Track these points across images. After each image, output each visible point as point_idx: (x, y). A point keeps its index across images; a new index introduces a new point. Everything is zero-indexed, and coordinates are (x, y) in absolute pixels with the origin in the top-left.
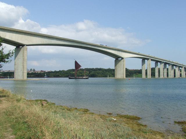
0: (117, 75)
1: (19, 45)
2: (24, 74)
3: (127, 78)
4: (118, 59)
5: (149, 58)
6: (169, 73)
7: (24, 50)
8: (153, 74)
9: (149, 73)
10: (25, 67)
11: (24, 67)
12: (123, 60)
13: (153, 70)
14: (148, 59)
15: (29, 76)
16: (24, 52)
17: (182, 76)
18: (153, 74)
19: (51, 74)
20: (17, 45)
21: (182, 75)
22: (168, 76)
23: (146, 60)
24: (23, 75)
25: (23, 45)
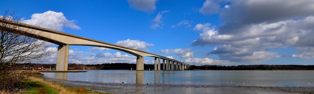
4: (138, 57)
7: (66, 48)
16: (66, 50)
25: (65, 45)
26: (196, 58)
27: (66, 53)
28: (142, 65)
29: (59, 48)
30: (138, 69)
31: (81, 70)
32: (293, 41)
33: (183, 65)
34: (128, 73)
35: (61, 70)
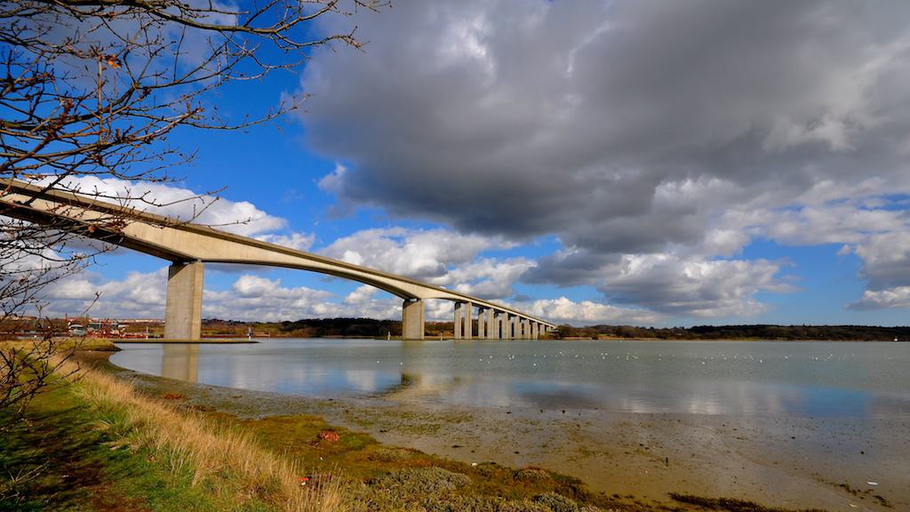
2: (194, 328)
3: (197, 322)
5: (469, 300)
6: (503, 330)
7: (195, 272)
8: (475, 333)
9: (469, 329)
10: (195, 311)
12: (419, 302)
13: (475, 324)
14: (466, 302)
15: (135, 334)
16: (194, 277)
18: (475, 333)
21: (525, 332)
22: (486, 335)
24: (190, 329)
25: (192, 260)
29: (172, 273)
30: (407, 337)
33: (535, 325)
35: (178, 337)
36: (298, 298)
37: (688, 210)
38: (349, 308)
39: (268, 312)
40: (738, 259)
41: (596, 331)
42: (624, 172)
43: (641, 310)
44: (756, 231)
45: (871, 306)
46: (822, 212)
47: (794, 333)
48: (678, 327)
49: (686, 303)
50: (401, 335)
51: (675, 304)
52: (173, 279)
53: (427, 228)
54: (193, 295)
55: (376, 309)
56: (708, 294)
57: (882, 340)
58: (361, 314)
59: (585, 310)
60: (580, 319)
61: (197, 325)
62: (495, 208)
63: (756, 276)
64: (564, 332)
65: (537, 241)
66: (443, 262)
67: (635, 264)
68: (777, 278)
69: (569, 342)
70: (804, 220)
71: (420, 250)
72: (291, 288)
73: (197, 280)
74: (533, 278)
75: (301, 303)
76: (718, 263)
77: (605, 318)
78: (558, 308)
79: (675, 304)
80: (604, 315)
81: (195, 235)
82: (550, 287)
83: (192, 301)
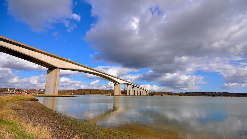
0: (115, 93)
1: (52, 67)
4: (116, 83)
7: (57, 72)
10: (56, 85)
11: (55, 86)
12: (119, 84)
15: (30, 93)
16: (57, 74)
17: (135, 95)
19: (42, 91)
20: (50, 67)
23: (129, 85)
25: (55, 68)
26: (230, 84)
27: (56, 76)
28: (119, 91)
29: (48, 72)
30: (115, 95)
31: (60, 94)
32: (34, 83)
33: (146, 91)
34: (35, 95)
35: (50, 94)
36: (77, 83)
37: (183, 64)
38: (90, 86)
39: (67, 87)
40: (194, 75)
41: (161, 94)
42: (167, 53)
43: (168, 88)
44: (198, 69)
45: (226, 87)
46: (215, 65)
47: (214, 95)
48: (181, 92)
49: (181, 86)
50: (113, 94)
51: (178, 87)
52: (48, 74)
53: (116, 66)
54: (56, 80)
55: (97, 87)
56: (186, 84)
57: (236, 96)
58: (93, 88)
59: (154, 88)
60: (152, 90)
61: (57, 90)
62: (133, 61)
63: (198, 80)
64: (153, 94)
65: (143, 70)
66: (119, 75)
67: (169, 76)
68: (203, 80)
69: (155, 96)
70: (210, 66)
71: (113, 71)
72: (75, 81)
73: (57, 75)
74: (141, 79)
75: (77, 85)
76: (189, 76)
77: (159, 90)
78: (147, 87)
79: (178, 87)
80: (158, 89)
81: (58, 60)
82: (145, 81)
83: (55, 82)
